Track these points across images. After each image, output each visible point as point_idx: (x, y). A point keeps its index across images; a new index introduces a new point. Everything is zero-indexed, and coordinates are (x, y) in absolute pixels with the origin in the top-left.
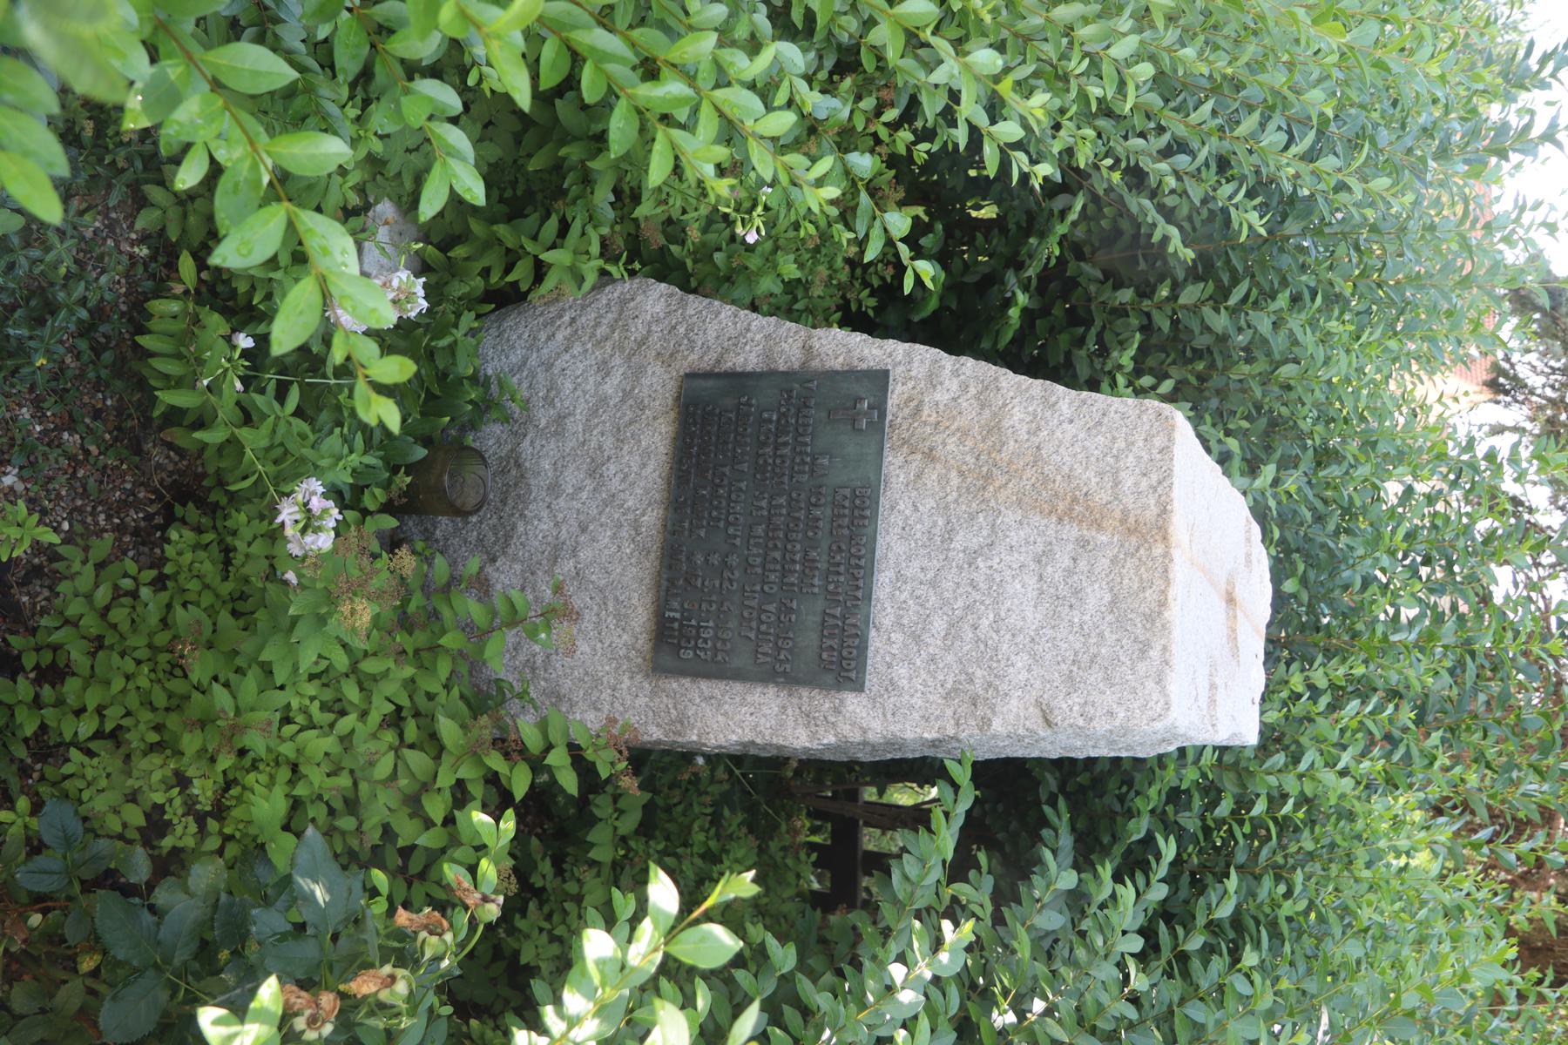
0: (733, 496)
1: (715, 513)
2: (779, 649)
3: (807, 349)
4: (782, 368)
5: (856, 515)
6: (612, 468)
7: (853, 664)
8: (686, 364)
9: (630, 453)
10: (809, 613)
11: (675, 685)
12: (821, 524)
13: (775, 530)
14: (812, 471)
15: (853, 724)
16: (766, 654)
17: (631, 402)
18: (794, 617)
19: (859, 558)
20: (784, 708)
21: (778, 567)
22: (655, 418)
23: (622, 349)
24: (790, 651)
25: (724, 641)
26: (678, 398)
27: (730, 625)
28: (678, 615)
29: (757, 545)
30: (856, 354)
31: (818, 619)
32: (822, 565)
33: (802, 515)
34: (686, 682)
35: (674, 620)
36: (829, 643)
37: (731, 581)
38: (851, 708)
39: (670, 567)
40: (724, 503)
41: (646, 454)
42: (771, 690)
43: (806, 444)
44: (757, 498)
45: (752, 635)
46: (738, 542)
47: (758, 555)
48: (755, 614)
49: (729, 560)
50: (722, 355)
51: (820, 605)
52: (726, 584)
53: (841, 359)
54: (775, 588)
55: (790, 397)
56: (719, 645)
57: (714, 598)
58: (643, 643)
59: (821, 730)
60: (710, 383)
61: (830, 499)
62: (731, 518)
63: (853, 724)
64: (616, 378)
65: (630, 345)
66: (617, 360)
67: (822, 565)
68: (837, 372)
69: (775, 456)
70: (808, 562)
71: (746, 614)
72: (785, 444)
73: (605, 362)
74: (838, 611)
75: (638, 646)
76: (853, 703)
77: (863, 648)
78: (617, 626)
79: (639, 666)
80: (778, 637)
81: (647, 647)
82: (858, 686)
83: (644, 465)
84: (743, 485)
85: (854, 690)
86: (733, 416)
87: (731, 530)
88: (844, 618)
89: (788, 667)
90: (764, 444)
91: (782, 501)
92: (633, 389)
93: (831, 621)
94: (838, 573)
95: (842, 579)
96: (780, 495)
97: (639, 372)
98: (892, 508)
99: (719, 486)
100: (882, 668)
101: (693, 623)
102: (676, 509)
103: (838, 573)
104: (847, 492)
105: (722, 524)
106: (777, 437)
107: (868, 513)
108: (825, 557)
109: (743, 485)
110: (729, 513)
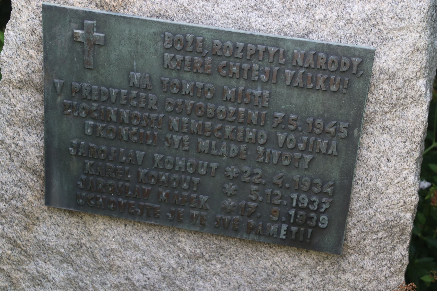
0: (169, 167)
1: (185, 185)
2: (324, 132)
3: (22, 85)
4: (41, 111)
5: (190, 48)
6: (137, 276)
7: (345, 60)
8: (36, 203)
9: (123, 259)
10: (289, 101)
11: (354, 232)
12: (199, 84)
13: (204, 130)
14: (146, 89)
15: (408, 61)
16: (329, 146)
17: (73, 256)
18: (292, 116)
19: (236, 48)
20: (384, 128)
21: (241, 128)
22: (90, 234)
23: (20, 262)
24: (326, 121)
25: (312, 184)
26: (72, 213)
27: (296, 177)
28: (284, 227)
29: (218, 147)
30: (27, 37)
31: (296, 92)
32: (242, 85)
33: (190, 102)
34: (351, 221)
35: (288, 231)
36: (321, 82)
37: (252, 174)
38: (391, 63)
39: (236, 231)
40: (176, 176)
41: (125, 245)
42: (365, 140)
43: (119, 93)
44: (172, 144)
45: (308, 157)
46: (214, 165)
47: (228, 147)
48: (287, 154)
49: (232, 175)
50: (27, 168)
51: (281, 90)
52: (255, 179)
53: (33, 53)
54: (262, 132)
55: (71, 106)
56: (316, 190)
57: (269, 191)
58: (309, 259)
59: (411, 93)
60: (56, 183)
61: (174, 74)
62: (191, 170)
63: (408, 61)
64: (50, 269)
65: (16, 255)
66: (31, 267)
67: (242, 85)
68: (46, 59)
69: (130, 124)
70: (238, 98)
71: (287, 162)
72: (118, 114)
73: (33, 279)
74: (289, 72)
75: (313, 263)
76: (384, 61)
77: (329, 49)
78: (291, 282)
79: (332, 264)
80: (311, 133)
81: (314, 255)
82: (369, 56)
83: (136, 247)
84: (158, 157)
85: (372, 60)
86: (89, 163)
87: (203, 171)
88: (297, 66)
89: (343, 125)
90: (118, 135)
91: (175, 120)
92: (59, 253)
93: (299, 80)
94: (250, 70)
95: (256, 66)
96: (170, 122)
97: (43, 248)
98: (186, 10)
99: (158, 180)
100: (351, 30)
101: (292, 212)
102: (180, 221)
103: (250, 70)
104: (168, 56)
105: (196, 179)
106: (111, 121)
107: (190, 37)
108: (233, 82)
109: (158, 157)
110: (186, 172)
